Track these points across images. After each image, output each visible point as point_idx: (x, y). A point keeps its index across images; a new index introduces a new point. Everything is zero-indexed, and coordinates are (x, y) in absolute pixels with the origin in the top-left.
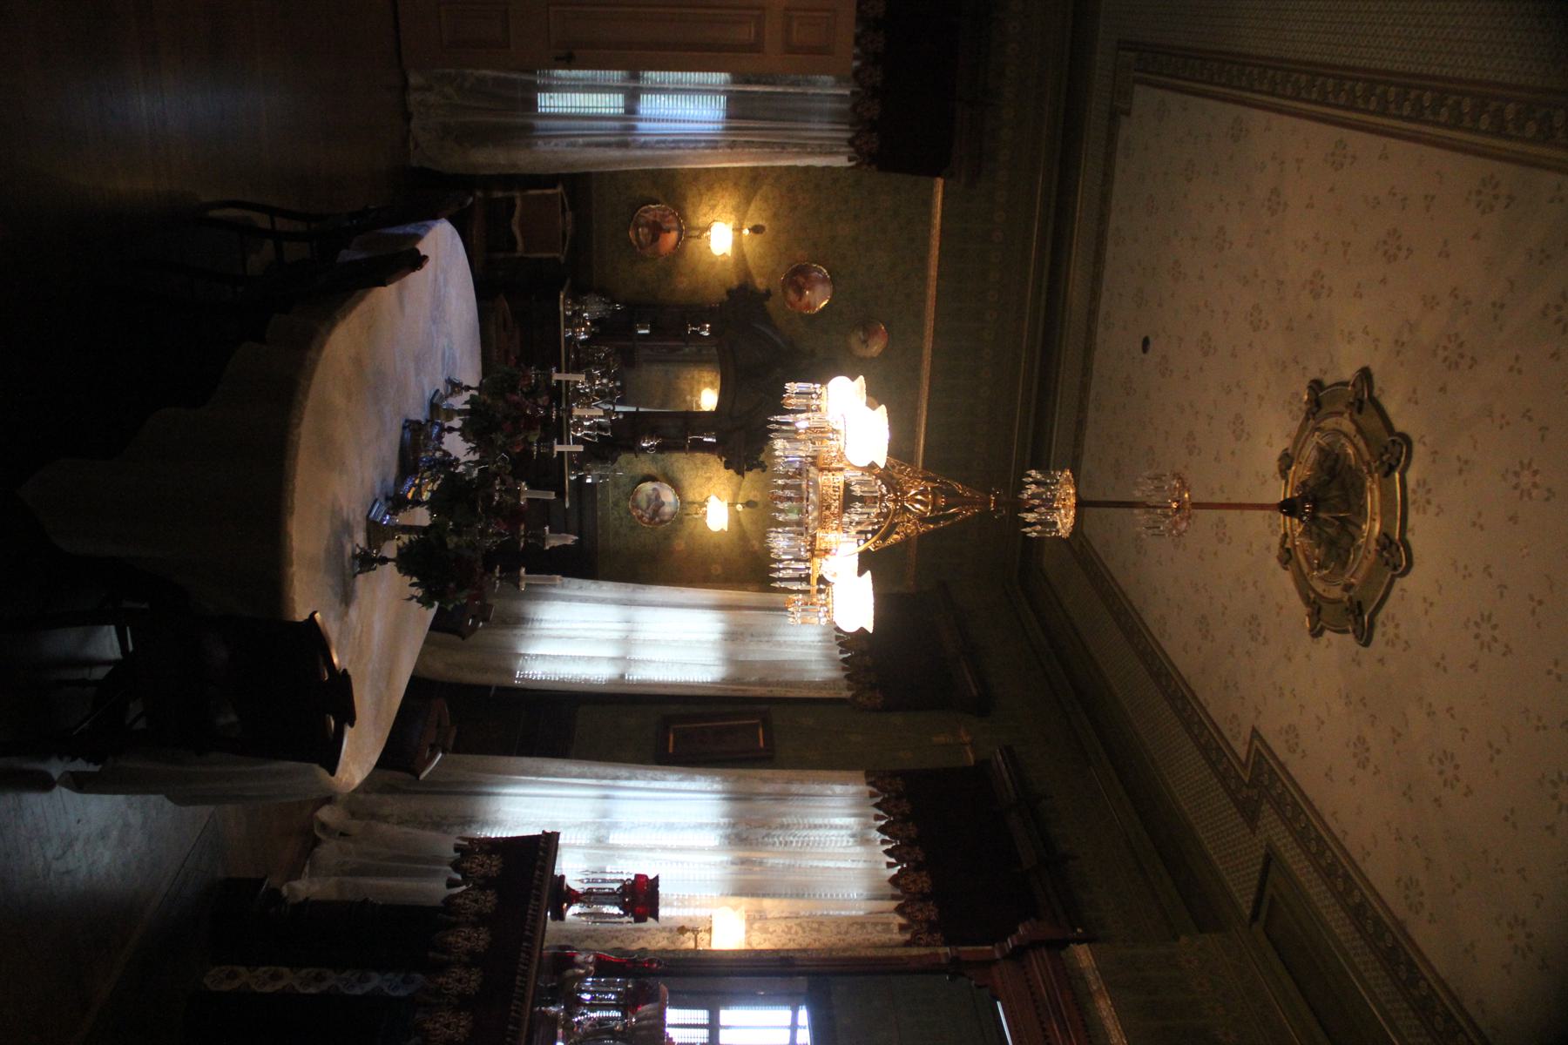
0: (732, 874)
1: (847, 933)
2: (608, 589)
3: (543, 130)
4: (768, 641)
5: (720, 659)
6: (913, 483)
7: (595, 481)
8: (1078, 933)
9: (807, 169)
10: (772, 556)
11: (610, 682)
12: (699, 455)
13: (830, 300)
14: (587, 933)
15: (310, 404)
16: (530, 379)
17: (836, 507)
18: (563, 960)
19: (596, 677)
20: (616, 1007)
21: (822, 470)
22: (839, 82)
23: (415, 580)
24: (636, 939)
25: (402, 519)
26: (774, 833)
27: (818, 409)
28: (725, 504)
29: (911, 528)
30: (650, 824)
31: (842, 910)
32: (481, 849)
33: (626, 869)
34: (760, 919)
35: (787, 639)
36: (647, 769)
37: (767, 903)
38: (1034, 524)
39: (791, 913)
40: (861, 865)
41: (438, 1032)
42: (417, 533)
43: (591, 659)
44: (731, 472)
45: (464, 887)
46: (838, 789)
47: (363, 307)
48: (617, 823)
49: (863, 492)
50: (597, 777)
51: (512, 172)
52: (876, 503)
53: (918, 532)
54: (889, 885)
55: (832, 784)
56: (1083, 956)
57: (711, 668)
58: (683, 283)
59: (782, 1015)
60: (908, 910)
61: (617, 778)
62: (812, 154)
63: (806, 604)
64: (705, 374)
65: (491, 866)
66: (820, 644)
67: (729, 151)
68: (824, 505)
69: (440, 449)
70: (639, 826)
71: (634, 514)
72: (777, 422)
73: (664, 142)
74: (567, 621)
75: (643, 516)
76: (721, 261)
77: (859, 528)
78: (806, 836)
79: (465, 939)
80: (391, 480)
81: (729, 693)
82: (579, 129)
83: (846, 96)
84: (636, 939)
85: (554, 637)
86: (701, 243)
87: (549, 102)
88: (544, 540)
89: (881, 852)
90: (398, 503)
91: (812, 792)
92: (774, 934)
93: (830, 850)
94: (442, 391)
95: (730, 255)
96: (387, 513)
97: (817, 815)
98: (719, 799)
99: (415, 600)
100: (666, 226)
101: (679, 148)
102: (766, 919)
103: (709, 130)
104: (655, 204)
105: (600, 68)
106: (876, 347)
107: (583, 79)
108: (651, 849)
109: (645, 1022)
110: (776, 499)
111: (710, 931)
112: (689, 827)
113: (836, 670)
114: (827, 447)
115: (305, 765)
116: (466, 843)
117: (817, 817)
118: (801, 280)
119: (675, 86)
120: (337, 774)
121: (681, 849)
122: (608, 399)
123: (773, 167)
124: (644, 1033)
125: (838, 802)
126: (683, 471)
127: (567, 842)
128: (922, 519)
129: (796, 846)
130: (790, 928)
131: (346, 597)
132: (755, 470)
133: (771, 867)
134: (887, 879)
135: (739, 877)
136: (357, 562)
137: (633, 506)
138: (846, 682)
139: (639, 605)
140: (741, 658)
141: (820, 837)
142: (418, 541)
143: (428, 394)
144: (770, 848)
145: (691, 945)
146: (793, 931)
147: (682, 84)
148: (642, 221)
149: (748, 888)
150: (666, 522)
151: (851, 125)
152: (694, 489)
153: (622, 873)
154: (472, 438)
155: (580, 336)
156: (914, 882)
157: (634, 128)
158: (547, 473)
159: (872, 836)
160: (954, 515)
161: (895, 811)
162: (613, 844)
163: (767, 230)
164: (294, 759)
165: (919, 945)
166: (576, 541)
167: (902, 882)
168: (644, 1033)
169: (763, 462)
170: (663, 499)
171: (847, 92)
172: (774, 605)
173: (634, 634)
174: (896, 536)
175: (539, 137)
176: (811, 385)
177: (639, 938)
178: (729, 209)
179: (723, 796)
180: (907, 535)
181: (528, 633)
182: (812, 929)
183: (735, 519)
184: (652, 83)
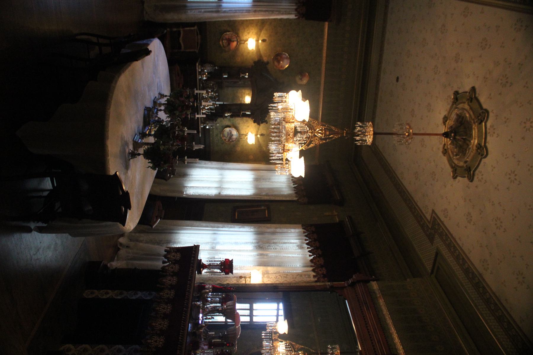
1: (295, 278)
2: (214, 164)
4: (269, 181)
6: (318, 127)
9: (281, 19)
10: (270, 152)
11: (216, 195)
12: (245, 118)
15: (113, 102)
18: (201, 287)
19: (211, 194)
20: (219, 303)
21: (287, 122)
23: (150, 161)
25: (145, 140)
26: (271, 245)
27: (285, 102)
28: (254, 135)
29: (317, 142)
30: (230, 242)
31: (294, 270)
32: (173, 251)
33: (222, 257)
34: (267, 274)
35: (275, 180)
36: (227, 224)
37: (270, 269)
44: (256, 124)
46: (293, 230)
47: (130, 68)
48: (219, 242)
49: (301, 130)
50: (212, 227)
52: (305, 133)
54: (310, 262)
55: (291, 229)
56: (374, 285)
57: (250, 190)
58: (239, 59)
59: (274, 305)
61: (218, 227)
62: (283, 14)
63: (282, 168)
66: (286, 182)
67: (254, 13)
68: (288, 134)
69: (157, 117)
71: (223, 138)
72: (272, 106)
75: (226, 139)
77: (300, 142)
78: (282, 246)
81: (256, 199)
85: (196, 180)
90: (143, 135)
91: (284, 232)
92: (272, 279)
93: (290, 251)
96: (140, 138)
97: (286, 239)
99: (150, 168)
100: (232, 40)
102: (269, 273)
106: (305, 81)
108: (230, 251)
109: (229, 307)
110: (271, 132)
112: (243, 243)
113: (292, 191)
116: (169, 249)
118: (279, 58)
121: (240, 251)
124: (228, 310)
125: (293, 235)
126: (239, 124)
128: (321, 139)
130: (277, 277)
131: (127, 167)
133: (270, 256)
137: (223, 136)
140: (260, 187)
142: (150, 148)
143: (153, 98)
144: (270, 250)
145: (244, 282)
146: (278, 278)
149: (263, 263)
150: (234, 141)
151: (296, 4)
152: (243, 130)
154: (168, 113)
156: (318, 261)
157: (221, 6)
158: (193, 124)
160: (332, 137)
169: (267, 121)
170: (233, 133)
172: (271, 169)
174: (312, 145)
177: (226, 280)
178: (254, 33)
179: (254, 233)
181: (188, 179)
182: (284, 277)
183: (257, 140)
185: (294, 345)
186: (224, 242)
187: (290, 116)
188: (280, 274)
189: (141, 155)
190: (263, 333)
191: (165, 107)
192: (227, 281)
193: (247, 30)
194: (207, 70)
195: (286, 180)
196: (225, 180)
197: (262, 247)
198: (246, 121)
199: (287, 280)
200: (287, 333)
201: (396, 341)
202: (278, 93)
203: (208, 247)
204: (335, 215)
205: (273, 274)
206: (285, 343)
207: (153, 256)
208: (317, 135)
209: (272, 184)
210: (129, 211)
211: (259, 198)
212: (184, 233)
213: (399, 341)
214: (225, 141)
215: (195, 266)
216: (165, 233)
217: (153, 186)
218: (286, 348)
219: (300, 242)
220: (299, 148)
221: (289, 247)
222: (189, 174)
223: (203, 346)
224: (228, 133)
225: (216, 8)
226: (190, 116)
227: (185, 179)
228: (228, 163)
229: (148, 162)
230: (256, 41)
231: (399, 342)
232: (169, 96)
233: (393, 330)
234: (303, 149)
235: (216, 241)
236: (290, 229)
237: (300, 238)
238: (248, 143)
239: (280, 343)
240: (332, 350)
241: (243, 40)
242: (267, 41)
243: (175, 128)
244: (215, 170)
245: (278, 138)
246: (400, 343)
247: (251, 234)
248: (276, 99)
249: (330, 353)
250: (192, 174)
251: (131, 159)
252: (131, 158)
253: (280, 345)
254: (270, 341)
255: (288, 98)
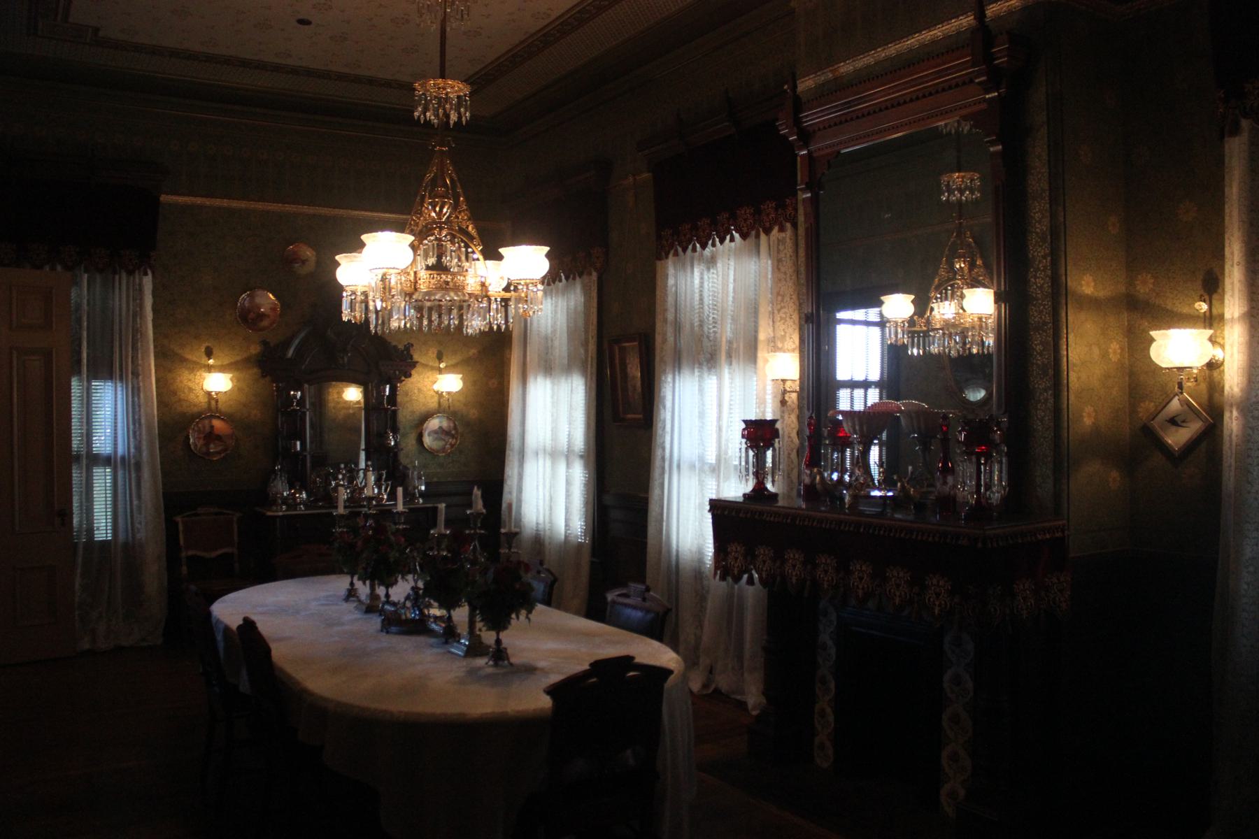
0: (739, 364)
1: (785, 273)
2: (511, 471)
3: (127, 535)
4: (552, 340)
5: (566, 379)
6: (426, 214)
7: (423, 483)
8: (788, 88)
9: (154, 310)
10: (487, 330)
11: (586, 466)
12: (399, 399)
13: (268, 291)
14: (786, 477)
15: (374, 705)
16: (342, 532)
17: (447, 277)
18: (812, 493)
19: (582, 478)
20: (843, 452)
21: (416, 289)
22: (76, 282)
23: (514, 616)
24: (790, 439)
25: (463, 629)
26: (706, 333)
27: (365, 294)
28: (440, 377)
29: (463, 216)
30: (700, 431)
31: (767, 278)
32: (723, 560)
33: (736, 444)
34: (775, 342)
35: (549, 325)
36: (656, 435)
37: (762, 336)
38: (459, 113)
39: (770, 318)
40: (732, 263)
41: (866, 586)
42: (475, 616)
43: (568, 483)
44: (413, 372)
45: (754, 572)
46: (671, 281)
47: (289, 669)
48: (699, 457)
49: (433, 255)
50: (663, 473)
51: (164, 559)
52: (442, 245)
53: (467, 210)
54: (747, 240)
55: (667, 286)
56: (806, 84)
57: (574, 385)
59: (841, 330)
60: (768, 225)
61: (663, 459)
62: (141, 306)
63: (526, 301)
64: (330, 398)
65: (736, 552)
66: (554, 298)
67: (140, 378)
68: (445, 287)
69: (404, 603)
70: (701, 439)
71: (449, 451)
72: (376, 327)
73: (134, 433)
74: (537, 502)
75: (451, 444)
76: (237, 382)
77: (463, 258)
78: (709, 307)
79: (794, 569)
80: (433, 640)
81: (594, 370)
82: (126, 504)
83: (88, 277)
84: (790, 439)
85: (551, 514)
86: (222, 399)
87: (103, 529)
88: (479, 514)
89: (722, 247)
90: (450, 634)
91: (673, 303)
92: (786, 330)
93: (720, 287)
94: (355, 604)
95: (231, 375)
96: (458, 642)
97: (692, 299)
98: (680, 376)
99: (530, 616)
100: (208, 430)
101: (140, 419)
102: (774, 337)
103: (123, 395)
104: (189, 439)
105: (71, 489)
106: (308, 253)
107: (81, 503)
108: (720, 429)
109: (857, 428)
110: (440, 328)
111: (784, 381)
112: (702, 400)
113: (574, 284)
114: (397, 283)
115: (665, 695)
116: (719, 572)
117: (694, 299)
118: (252, 315)
119: (85, 424)
120: (672, 668)
121: (720, 406)
122: (355, 473)
123: (154, 340)
124: (865, 429)
125: (682, 282)
126: (413, 412)
127: (714, 491)
128: (455, 207)
129: (717, 315)
130: (782, 318)
131: (529, 670)
132: (412, 352)
133: (733, 333)
134: (743, 241)
135: (741, 359)
136: (500, 663)
137: (443, 452)
138: (585, 277)
139: (524, 449)
140: (565, 361)
141: (709, 296)
142: (482, 613)
143: (358, 615)
144: (718, 335)
145: (794, 396)
146: (784, 316)
147: (82, 418)
148: (204, 449)
149: (749, 352)
150: (455, 425)
151: (115, 272)
152: (428, 403)
153: (740, 449)
154: (394, 578)
155: (303, 498)
156: (745, 220)
157: (123, 458)
158: (422, 519)
159: (709, 254)
160: (452, 180)
161: (688, 236)
162: (716, 460)
163: (210, 345)
164: (661, 702)
165: (796, 217)
166: (478, 488)
167: (745, 230)
168: (865, 429)
169: (405, 346)
170: (436, 427)
171: (86, 276)
172: (522, 336)
173: (547, 448)
174: (470, 228)
175: (134, 537)
176: (344, 300)
177: (789, 437)
178: (191, 376)
179: (677, 373)
180: (469, 219)
181: (548, 533)
182: (782, 301)
183: (451, 369)
184: (82, 444)
185: (939, 280)
186: (699, 444)
187: (401, 279)
188: (776, 312)
189: (500, 637)
190: (912, 353)
191: (379, 585)
192: (792, 435)
193: (184, 393)
194: (283, 491)
195: (549, 300)
196: (549, 443)
197: (711, 355)
198: (407, 395)
199: (791, 295)
200: (913, 297)
201: (939, 34)
202: (342, 312)
203: (710, 483)
204: (635, 179)
205: (776, 326)
206: (934, 301)
207: (732, 607)
208: (445, 217)
209: (558, 333)
210: (637, 660)
211: (592, 362)
212: (678, 538)
213: (939, 28)
214: (456, 446)
215: (759, 507)
216: (677, 582)
217: (567, 610)
218: (946, 299)
219: (699, 264)
220: (478, 259)
221: (711, 289)
222: (535, 532)
223: (948, 486)
224: (436, 439)
225: (130, 472)
226: (400, 524)
227: (547, 542)
228: (509, 439)
229: (516, 620)
230: (210, 372)
231: (943, 27)
232: (352, 578)
233: (913, 41)
234: (481, 251)
235: (697, 463)
236: (669, 288)
237: (689, 268)
238: (460, 390)
239: (935, 312)
240: (954, 190)
241: (209, 402)
242: (207, 344)
243: (434, 557)
244: (525, 470)
245: (455, 312)
246: (945, 23)
247: (680, 380)
248: (358, 314)
249: (959, 195)
250: (534, 524)
251: (508, 659)
252: (506, 662)
253: (939, 312)
254: (930, 336)
255: (355, 286)
